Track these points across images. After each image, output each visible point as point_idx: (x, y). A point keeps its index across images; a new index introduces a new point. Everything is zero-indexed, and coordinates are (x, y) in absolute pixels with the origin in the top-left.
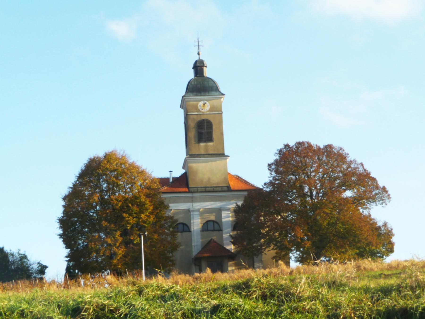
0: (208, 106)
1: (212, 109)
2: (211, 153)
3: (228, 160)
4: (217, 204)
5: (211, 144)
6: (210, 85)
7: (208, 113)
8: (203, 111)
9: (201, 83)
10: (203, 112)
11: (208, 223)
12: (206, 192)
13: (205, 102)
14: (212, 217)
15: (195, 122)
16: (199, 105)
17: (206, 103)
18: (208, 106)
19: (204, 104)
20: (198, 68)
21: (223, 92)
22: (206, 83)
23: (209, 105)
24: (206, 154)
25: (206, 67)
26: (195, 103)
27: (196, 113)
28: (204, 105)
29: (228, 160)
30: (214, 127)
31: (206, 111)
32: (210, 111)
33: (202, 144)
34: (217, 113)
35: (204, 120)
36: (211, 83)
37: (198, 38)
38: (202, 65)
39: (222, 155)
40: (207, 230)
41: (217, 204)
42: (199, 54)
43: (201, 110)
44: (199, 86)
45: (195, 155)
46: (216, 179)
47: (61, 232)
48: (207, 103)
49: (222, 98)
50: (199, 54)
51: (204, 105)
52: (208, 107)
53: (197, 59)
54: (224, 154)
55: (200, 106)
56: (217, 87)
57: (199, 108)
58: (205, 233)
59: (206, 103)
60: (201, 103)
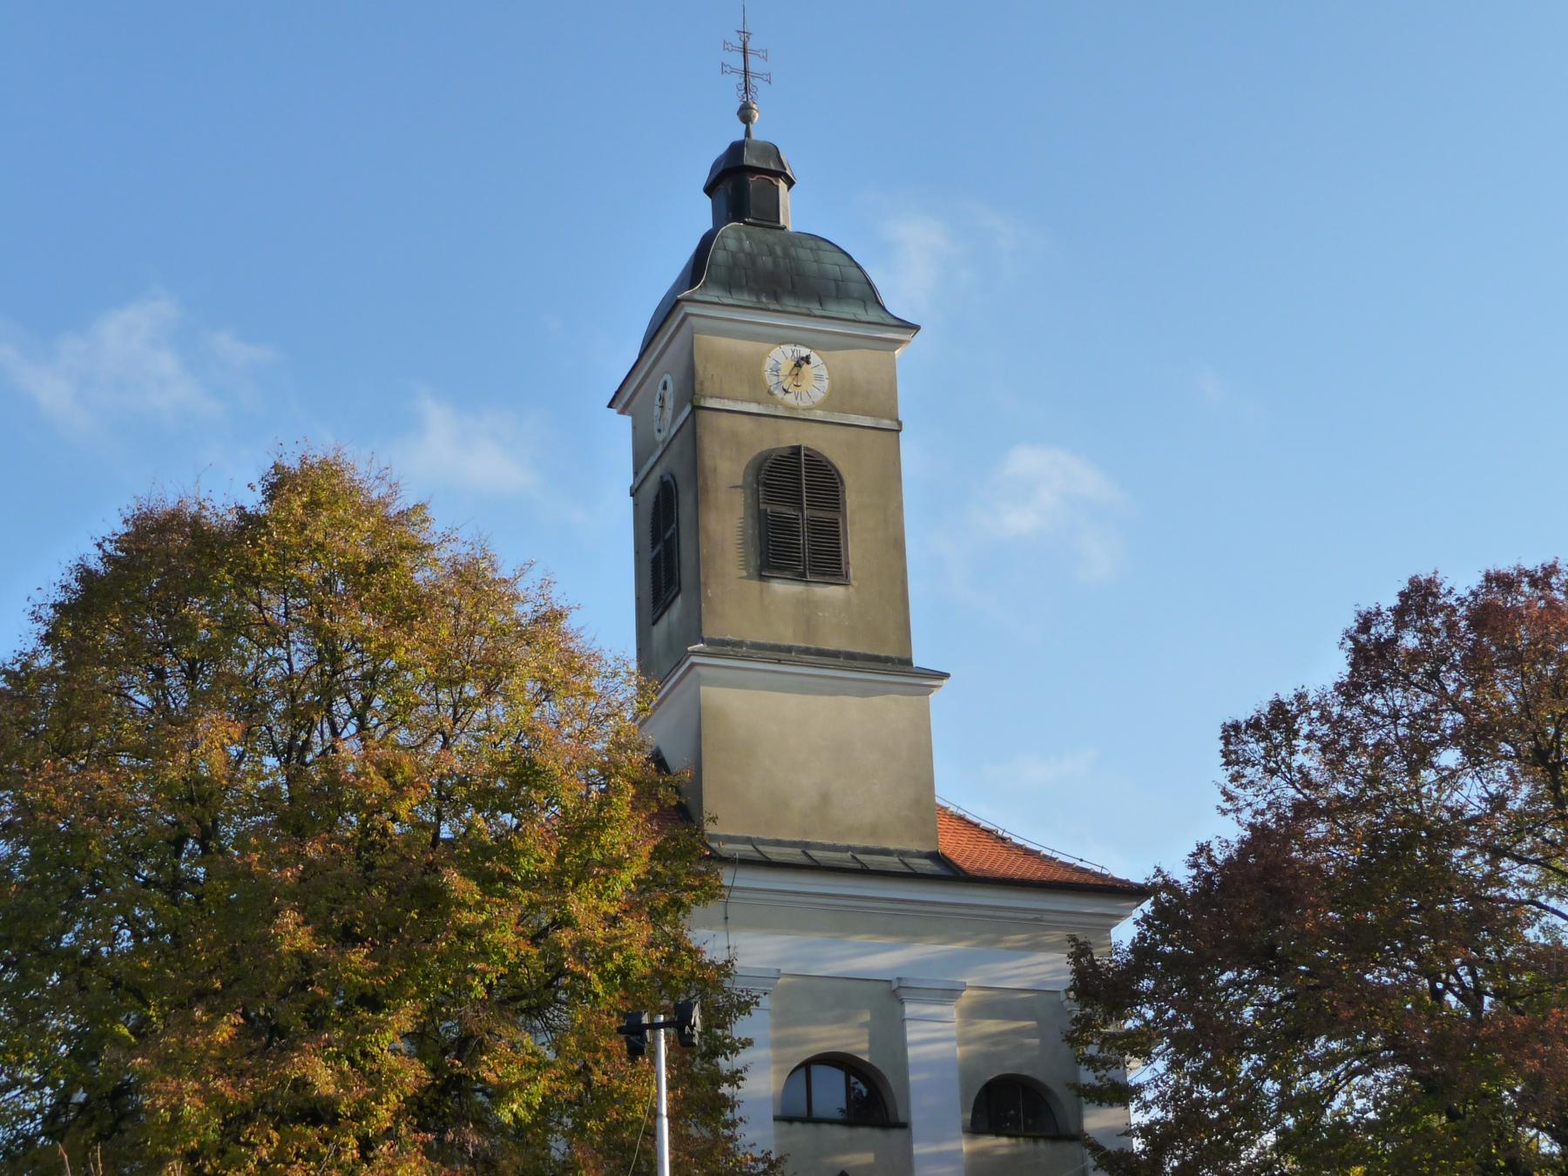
0: (819, 377)
1: (843, 394)
2: (832, 645)
3: (934, 698)
4: (882, 958)
5: (834, 592)
6: (832, 270)
7: (819, 414)
8: (790, 399)
9: (779, 250)
10: (793, 408)
11: (817, 1071)
12: (864, 872)
13: (804, 352)
14: (851, 1038)
15: (747, 457)
16: (769, 364)
17: (807, 360)
18: (819, 377)
19: (798, 365)
20: (753, 179)
21: (896, 306)
22: (803, 254)
23: (825, 373)
24: (807, 651)
25: (791, 183)
26: (745, 347)
27: (754, 408)
28: (782, 374)
29: (939, 700)
30: (853, 498)
31: (805, 402)
32: (826, 405)
33: (782, 589)
34: (868, 421)
35: (796, 450)
36: (830, 258)
37: (744, 33)
38: (772, 166)
39: (890, 664)
40: (810, 1119)
41: (882, 958)
42: (745, 115)
43: (779, 394)
44: (767, 261)
45: (740, 644)
46: (864, 814)
47: (95, 563)
48: (814, 358)
49: (901, 342)
50: (745, 115)
51: (782, 374)
52: (815, 387)
53: (740, 136)
54: (909, 662)
55: (776, 371)
56: (869, 283)
57: (770, 380)
58: (785, 1126)
59: (807, 360)
60: (783, 356)
